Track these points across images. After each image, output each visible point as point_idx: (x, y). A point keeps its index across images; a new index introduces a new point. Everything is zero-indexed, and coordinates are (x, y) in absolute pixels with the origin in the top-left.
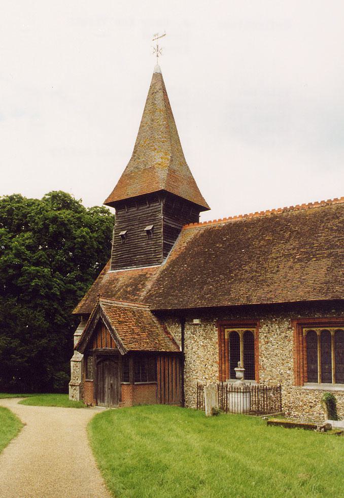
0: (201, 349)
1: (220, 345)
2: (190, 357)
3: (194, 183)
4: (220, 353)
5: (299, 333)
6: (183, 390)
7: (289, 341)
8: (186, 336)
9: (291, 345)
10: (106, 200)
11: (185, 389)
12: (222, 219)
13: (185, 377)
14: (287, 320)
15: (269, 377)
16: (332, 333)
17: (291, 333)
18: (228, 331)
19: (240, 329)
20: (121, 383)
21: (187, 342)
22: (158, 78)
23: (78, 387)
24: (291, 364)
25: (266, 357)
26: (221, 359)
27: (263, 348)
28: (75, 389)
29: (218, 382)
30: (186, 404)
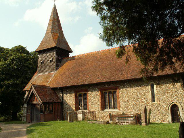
22: (55, 9)
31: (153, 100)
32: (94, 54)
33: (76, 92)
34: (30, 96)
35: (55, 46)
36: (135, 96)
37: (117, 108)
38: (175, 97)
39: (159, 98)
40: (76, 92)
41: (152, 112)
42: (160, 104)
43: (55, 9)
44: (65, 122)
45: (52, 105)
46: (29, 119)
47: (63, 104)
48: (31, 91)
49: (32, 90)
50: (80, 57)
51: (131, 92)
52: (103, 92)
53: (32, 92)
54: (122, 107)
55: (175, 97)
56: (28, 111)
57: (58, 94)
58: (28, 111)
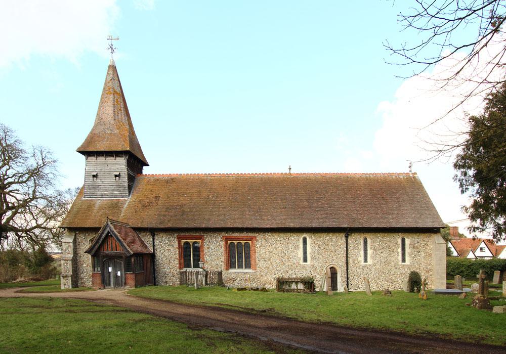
0: (167, 251)
1: (179, 249)
2: (159, 255)
3: (140, 147)
4: (179, 254)
5: (227, 243)
6: (154, 275)
7: (221, 247)
8: (155, 243)
9: (223, 250)
10: (79, 148)
11: (156, 274)
12: (461, 189)
13: (155, 267)
14: (220, 237)
15: (210, 266)
16: (243, 244)
17: (223, 244)
18: (183, 241)
19: (191, 240)
20: (66, 284)
21: (156, 247)
22: (113, 68)
23: (70, 278)
24: (223, 259)
25: (208, 256)
26: (179, 257)
27: (206, 251)
28: (67, 279)
29: (178, 270)
30: (157, 283)
31: (305, 260)
32: (220, 179)
33: (181, 238)
34: (101, 240)
35: (128, 149)
36: (280, 252)
37: (250, 267)
38: (334, 258)
39: (313, 258)
40: (181, 238)
41: (259, 267)
42: (313, 266)
43: (113, 68)
44: (257, 305)
45: (143, 258)
46: (98, 281)
47: (155, 256)
48: (106, 232)
49: (108, 229)
50: (171, 181)
51: (274, 246)
52: (183, 241)
53: (109, 232)
54: (259, 267)
55: (334, 258)
56: (94, 269)
57: (143, 239)
58: (94, 269)
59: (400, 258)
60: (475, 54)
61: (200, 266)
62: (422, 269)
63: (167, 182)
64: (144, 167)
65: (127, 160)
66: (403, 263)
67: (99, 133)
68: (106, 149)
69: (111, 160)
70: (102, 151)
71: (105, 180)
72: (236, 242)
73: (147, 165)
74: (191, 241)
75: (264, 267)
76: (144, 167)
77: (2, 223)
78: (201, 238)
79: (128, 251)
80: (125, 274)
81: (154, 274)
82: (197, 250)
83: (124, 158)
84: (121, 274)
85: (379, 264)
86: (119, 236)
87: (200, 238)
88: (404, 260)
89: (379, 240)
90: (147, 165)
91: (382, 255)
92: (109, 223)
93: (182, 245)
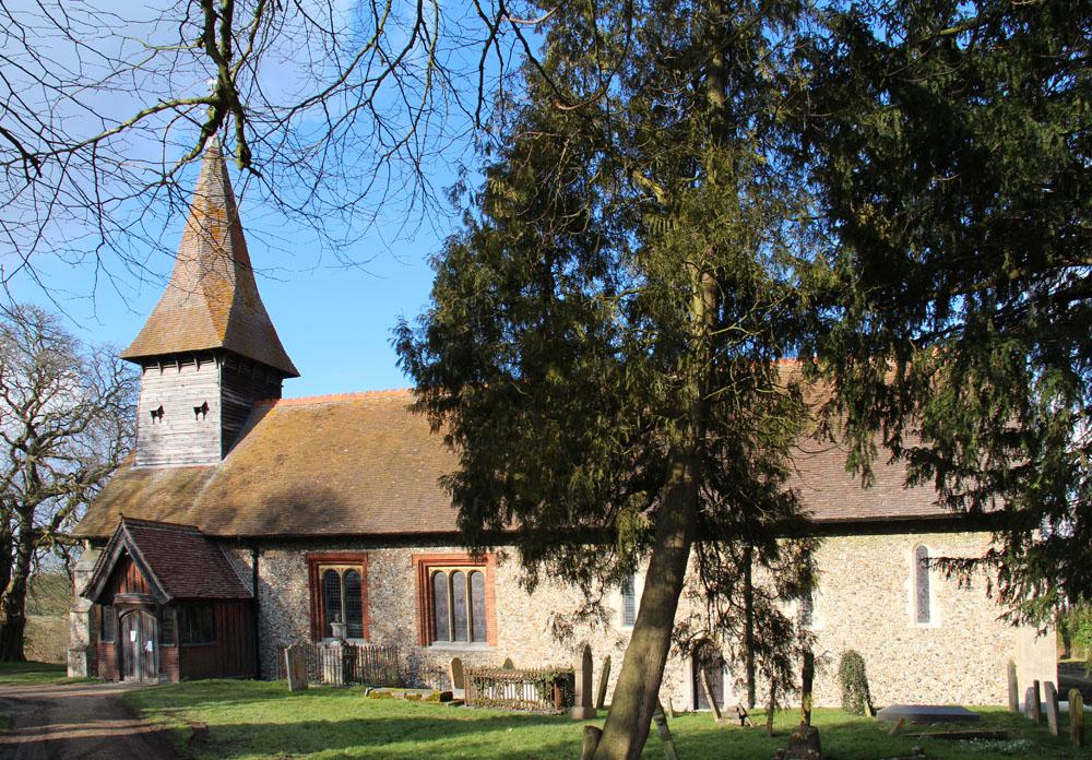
3: (273, 333)
7: (410, 584)
11: (261, 652)
13: (260, 635)
30: (263, 675)
49: (122, 543)
53: (124, 550)
59: (912, 608)
60: (349, 71)
61: (334, 634)
62: (982, 640)
63: (316, 416)
64: (285, 382)
65: (222, 369)
66: (923, 625)
67: (169, 311)
68: (178, 349)
69: (189, 370)
70: (168, 354)
71: (179, 422)
72: (341, 568)
73: (294, 374)
74: (341, 568)
75: (518, 637)
76: (285, 382)
77: (503, 498)
78: (361, 561)
79: (160, 593)
80: (161, 648)
81: (258, 652)
82: (356, 587)
83: (215, 366)
84: (154, 648)
85: (845, 627)
86: (142, 558)
87: (360, 561)
88: (924, 614)
89: (845, 556)
90: (294, 374)
91: (855, 600)
92: (124, 526)
93: (321, 577)
